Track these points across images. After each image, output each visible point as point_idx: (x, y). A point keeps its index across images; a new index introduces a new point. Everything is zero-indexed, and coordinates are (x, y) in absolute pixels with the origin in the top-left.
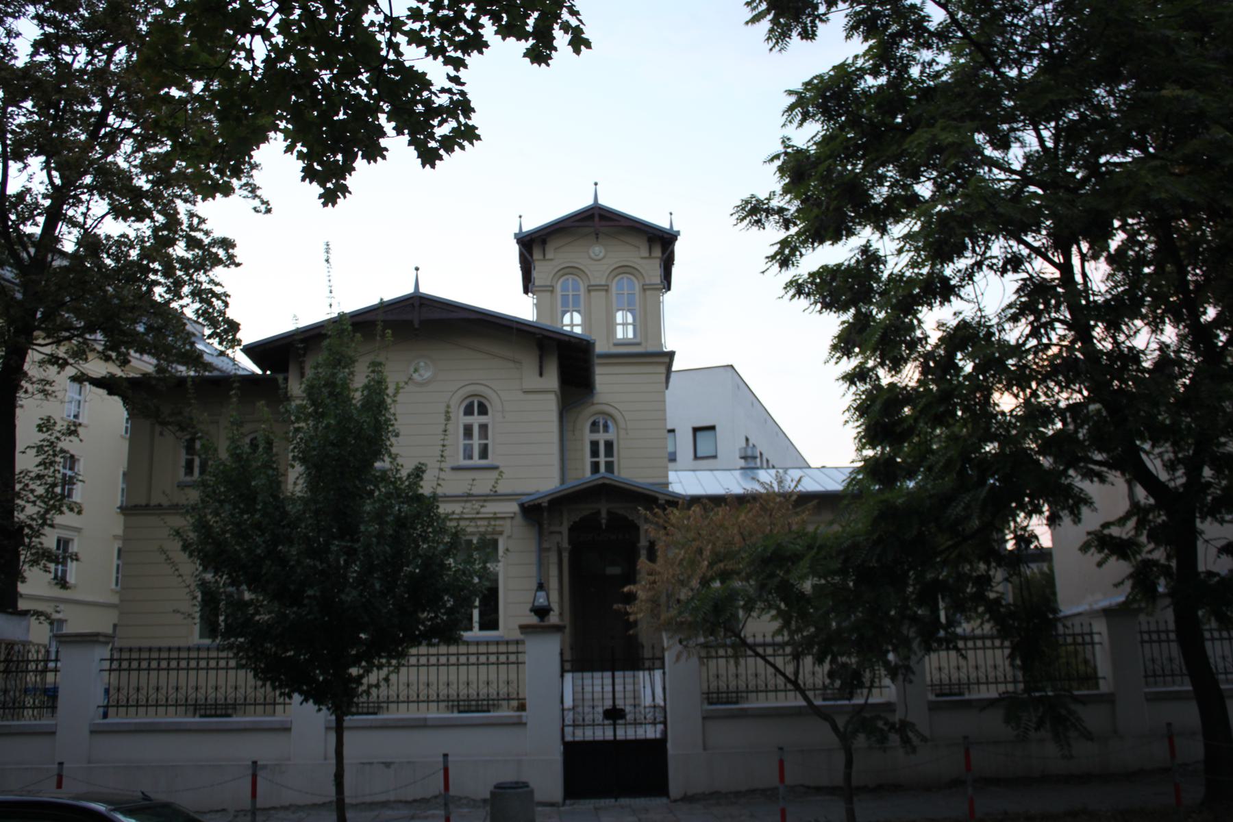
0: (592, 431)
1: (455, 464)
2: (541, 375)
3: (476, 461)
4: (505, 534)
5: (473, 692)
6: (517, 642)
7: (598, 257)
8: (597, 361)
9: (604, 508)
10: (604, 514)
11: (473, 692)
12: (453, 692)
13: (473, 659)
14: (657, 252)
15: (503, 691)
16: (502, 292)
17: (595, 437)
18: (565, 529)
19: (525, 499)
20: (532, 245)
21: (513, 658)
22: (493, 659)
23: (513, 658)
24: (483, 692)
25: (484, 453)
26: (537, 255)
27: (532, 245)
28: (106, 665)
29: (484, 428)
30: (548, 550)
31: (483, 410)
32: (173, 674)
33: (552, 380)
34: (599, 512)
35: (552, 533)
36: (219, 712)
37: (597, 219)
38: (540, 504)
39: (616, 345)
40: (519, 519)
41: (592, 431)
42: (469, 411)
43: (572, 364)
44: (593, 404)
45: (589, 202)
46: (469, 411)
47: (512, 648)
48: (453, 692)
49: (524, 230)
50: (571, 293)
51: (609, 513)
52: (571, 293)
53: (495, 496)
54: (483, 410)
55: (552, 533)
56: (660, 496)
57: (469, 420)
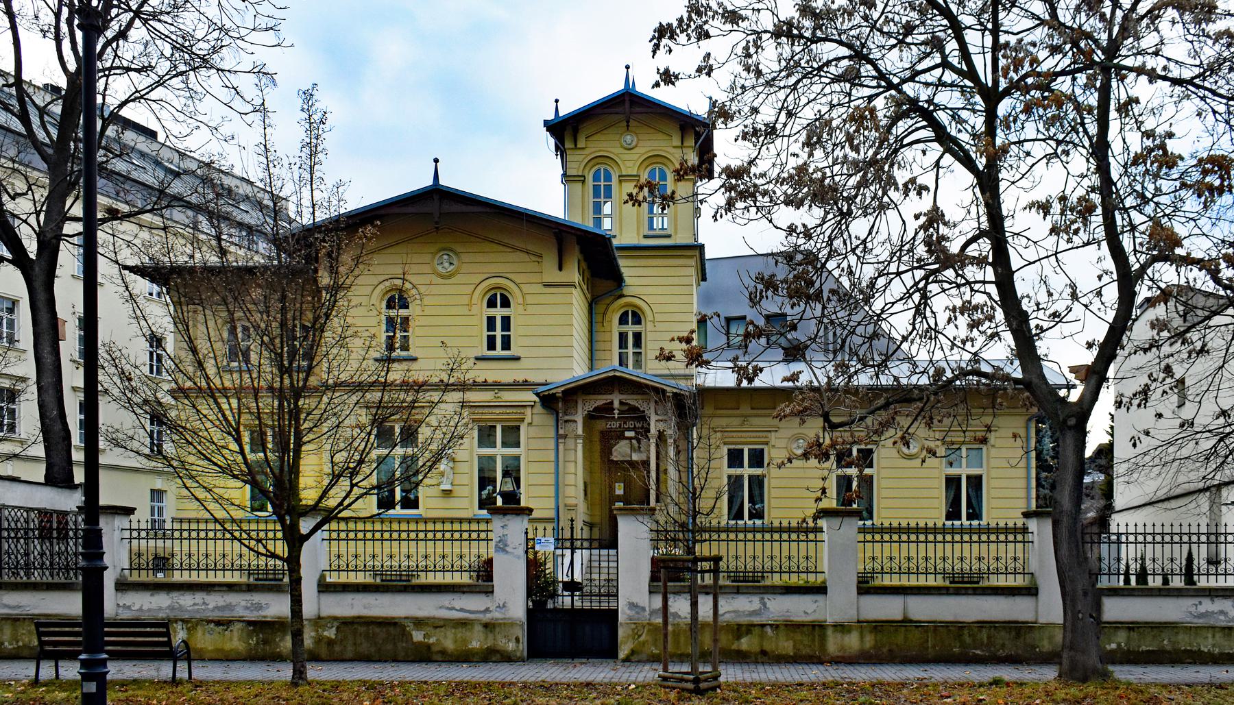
0: (489, 306)
1: (480, 355)
2: (560, 269)
3: (499, 351)
4: (526, 421)
5: (966, 567)
6: (487, 521)
7: (631, 153)
8: (617, 254)
9: (616, 399)
10: (616, 404)
11: (966, 567)
12: (948, 567)
13: (457, 536)
14: (690, 142)
15: (767, 566)
16: (535, 183)
17: (624, 328)
18: (579, 418)
19: (541, 389)
20: (565, 130)
21: (483, 535)
22: (466, 535)
23: (483, 535)
24: (957, 567)
25: (506, 344)
26: (568, 144)
27: (565, 130)
28: (127, 534)
29: (506, 321)
30: (565, 437)
31: (506, 303)
32: (185, 542)
33: (573, 274)
34: (612, 403)
35: (566, 421)
36: (36, 577)
37: (627, 104)
38: (554, 394)
39: (645, 237)
40: (539, 408)
41: (489, 306)
42: (491, 304)
43: (597, 260)
44: (622, 296)
45: (618, 86)
46: (491, 304)
47: (483, 526)
48: (948, 567)
49: (561, 114)
50: (602, 183)
51: (621, 403)
52: (602, 183)
53: (525, 385)
54: (506, 303)
55: (566, 421)
56: (668, 389)
57: (492, 312)
